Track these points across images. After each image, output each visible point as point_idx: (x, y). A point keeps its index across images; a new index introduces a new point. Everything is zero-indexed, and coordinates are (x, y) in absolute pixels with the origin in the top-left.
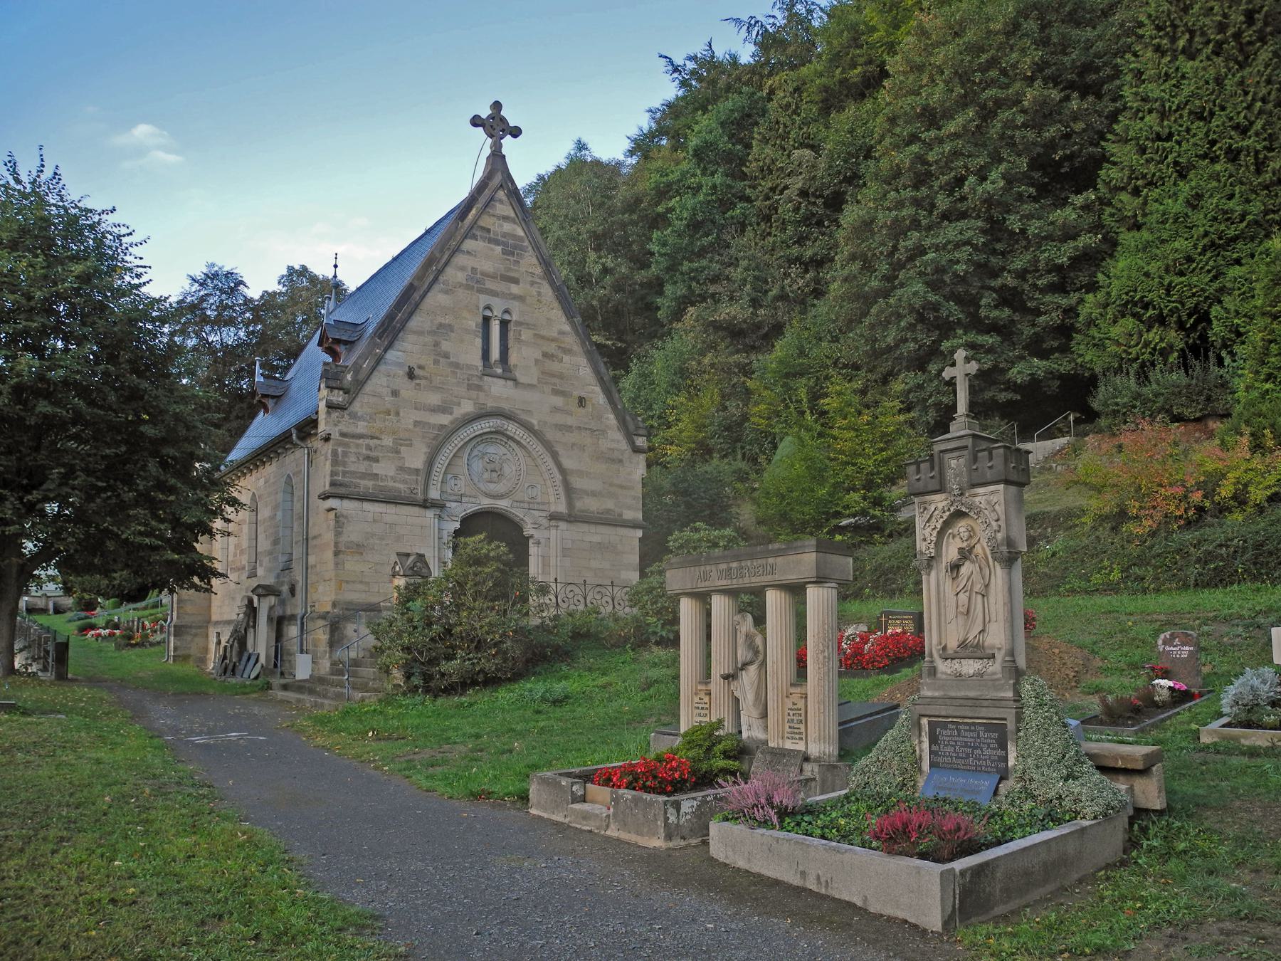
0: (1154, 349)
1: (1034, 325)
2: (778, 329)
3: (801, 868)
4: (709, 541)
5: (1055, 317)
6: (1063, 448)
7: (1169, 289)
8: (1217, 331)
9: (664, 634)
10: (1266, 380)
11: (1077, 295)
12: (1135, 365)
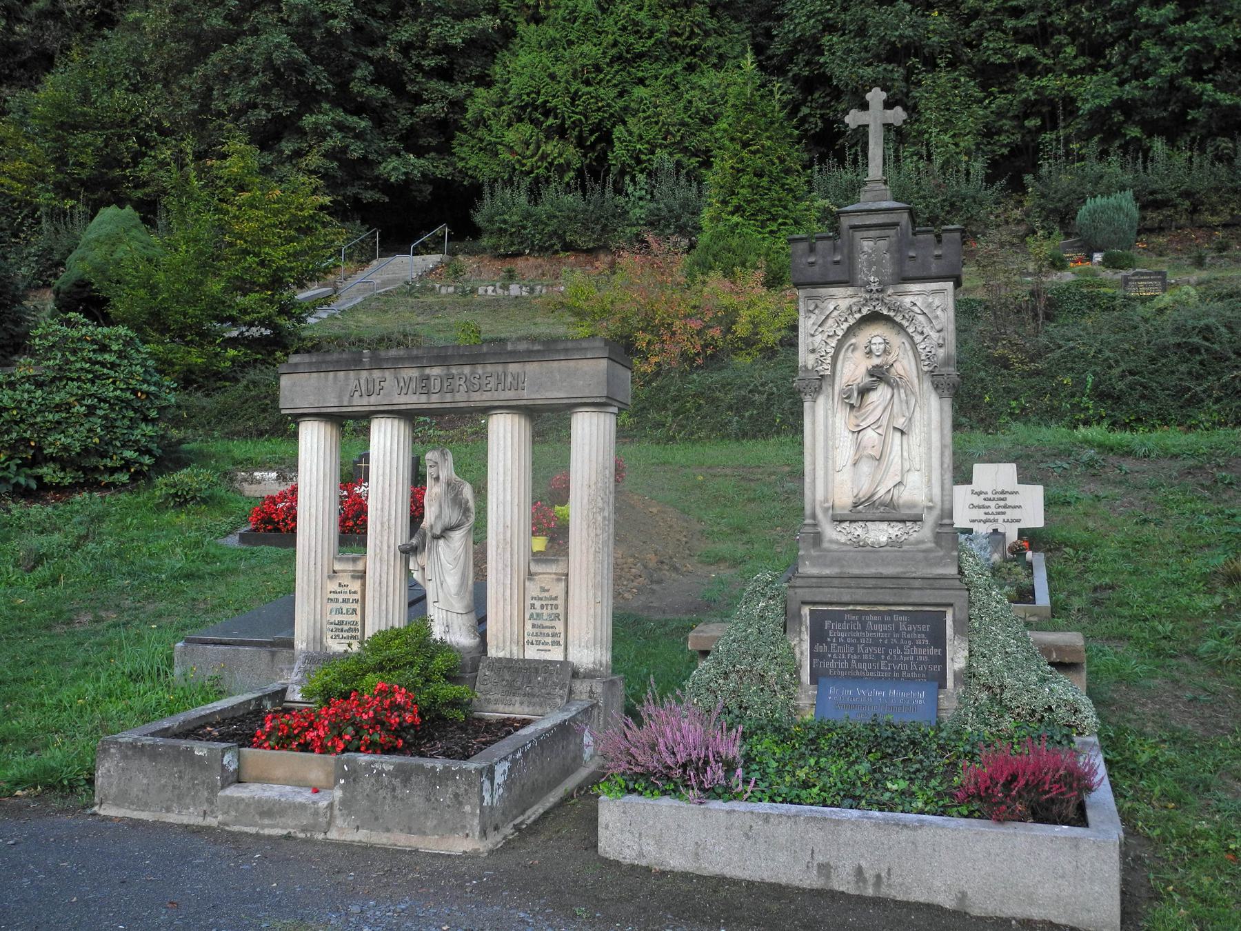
0: (551, 164)
1: (412, 114)
2: (46, 61)
3: (820, 858)
4: (94, 342)
5: (439, 109)
6: (436, 268)
7: (575, 97)
8: (618, 155)
9: (22, 480)
10: (733, 213)
11: (466, 87)
12: (528, 180)
